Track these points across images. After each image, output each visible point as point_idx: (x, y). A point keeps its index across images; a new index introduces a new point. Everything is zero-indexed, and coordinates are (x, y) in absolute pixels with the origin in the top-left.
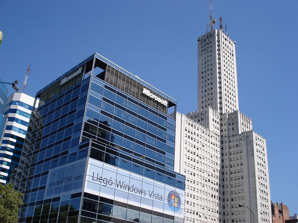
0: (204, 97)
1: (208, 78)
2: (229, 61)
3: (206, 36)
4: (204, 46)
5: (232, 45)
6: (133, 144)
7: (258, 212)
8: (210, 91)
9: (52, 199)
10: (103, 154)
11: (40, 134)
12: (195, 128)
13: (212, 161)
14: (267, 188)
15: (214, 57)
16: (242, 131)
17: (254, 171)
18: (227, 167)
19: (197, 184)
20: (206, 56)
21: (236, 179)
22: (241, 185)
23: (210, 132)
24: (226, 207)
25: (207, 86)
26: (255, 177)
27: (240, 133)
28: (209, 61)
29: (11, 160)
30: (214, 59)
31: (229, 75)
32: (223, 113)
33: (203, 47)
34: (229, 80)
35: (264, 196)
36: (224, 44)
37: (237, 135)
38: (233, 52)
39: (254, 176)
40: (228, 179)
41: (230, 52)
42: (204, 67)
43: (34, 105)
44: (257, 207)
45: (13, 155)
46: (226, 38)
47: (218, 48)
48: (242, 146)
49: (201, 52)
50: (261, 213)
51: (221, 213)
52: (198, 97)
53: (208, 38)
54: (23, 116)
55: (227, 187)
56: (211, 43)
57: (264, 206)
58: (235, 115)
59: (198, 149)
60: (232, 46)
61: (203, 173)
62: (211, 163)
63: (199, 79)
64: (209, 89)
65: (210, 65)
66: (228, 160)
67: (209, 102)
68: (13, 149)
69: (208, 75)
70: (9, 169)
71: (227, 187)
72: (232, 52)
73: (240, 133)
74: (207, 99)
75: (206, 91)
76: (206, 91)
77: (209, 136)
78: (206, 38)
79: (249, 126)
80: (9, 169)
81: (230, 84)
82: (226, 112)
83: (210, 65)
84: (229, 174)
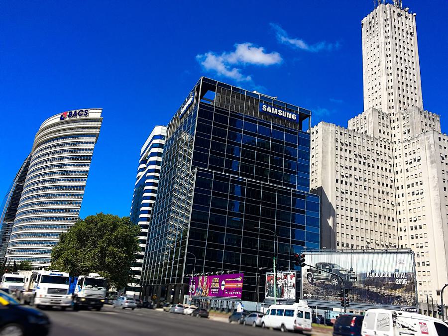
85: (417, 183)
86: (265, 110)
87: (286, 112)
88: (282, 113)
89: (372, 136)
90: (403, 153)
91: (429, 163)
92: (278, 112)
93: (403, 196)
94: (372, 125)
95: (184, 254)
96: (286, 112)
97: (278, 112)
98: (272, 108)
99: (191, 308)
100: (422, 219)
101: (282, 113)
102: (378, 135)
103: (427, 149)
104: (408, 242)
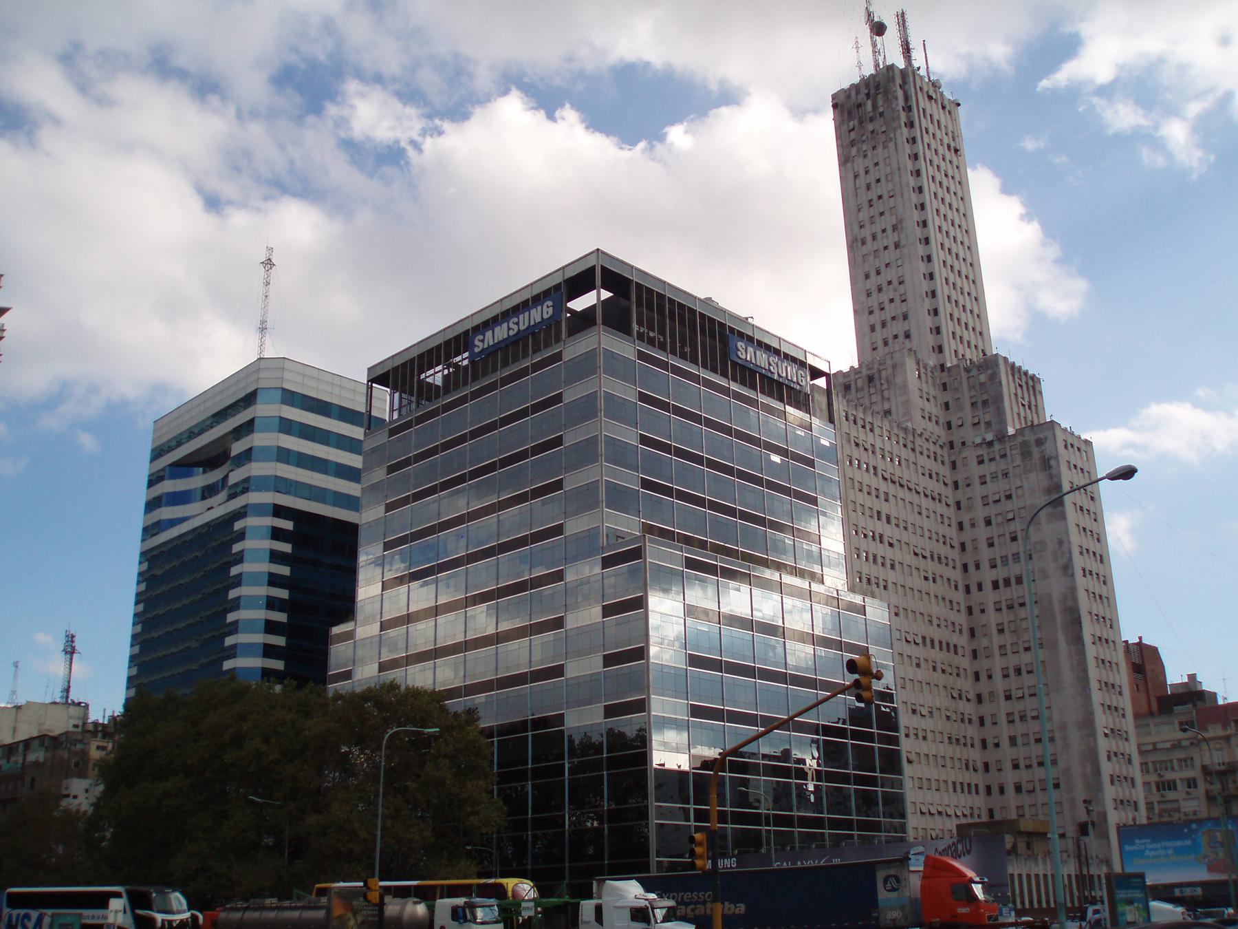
1: (893, 304)
2: (946, 175)
3: (864, 91)
4: (856, 128)
5: (949, 112)
6: (668, 418)
8: (895, 290)
9: (453, 340)
12: (863, 427)
13: (945, 623)
14: (1098, 520)
15: (899, 169)
16: (1018, 427)
18: (1000, 647)
19: (921, 788)
20: (869, 163)
23: (916, 436)
24: (958, 464)
25: (877, 220)
27: (1011, 431)
28: (883, 180)
30: (900, 177)
31: (948, 191)
32: (949, 365)
33: (853, 130)
34: (951, 229)
35: (1114, 701)
36: (925, 117)
38: (957, 139)
41: (946, 141)
42: (866, 205)
45: (287, 643)
46: (930, 94)
47: (914, 165)
50: (1106, 735)
51: (941, 423)
53: (868, 95)
54: (287, 479)
57: (1098, 597)
58: (989, 372)
59: (891, 545)
60: (961, 202)
62: (918, 454)
64: (890, 283)
65: (885, 196)
68: (289, 530)
69: (884, 231)
71: (960, 426)
72: (954, 140)
73: (1011, 431)
76: (874, 237)
77: (913, 450)
78: (862, 97)
79: (1033, 403)
81: (953, 225)
82: (955, 362)
83: (895, 282)
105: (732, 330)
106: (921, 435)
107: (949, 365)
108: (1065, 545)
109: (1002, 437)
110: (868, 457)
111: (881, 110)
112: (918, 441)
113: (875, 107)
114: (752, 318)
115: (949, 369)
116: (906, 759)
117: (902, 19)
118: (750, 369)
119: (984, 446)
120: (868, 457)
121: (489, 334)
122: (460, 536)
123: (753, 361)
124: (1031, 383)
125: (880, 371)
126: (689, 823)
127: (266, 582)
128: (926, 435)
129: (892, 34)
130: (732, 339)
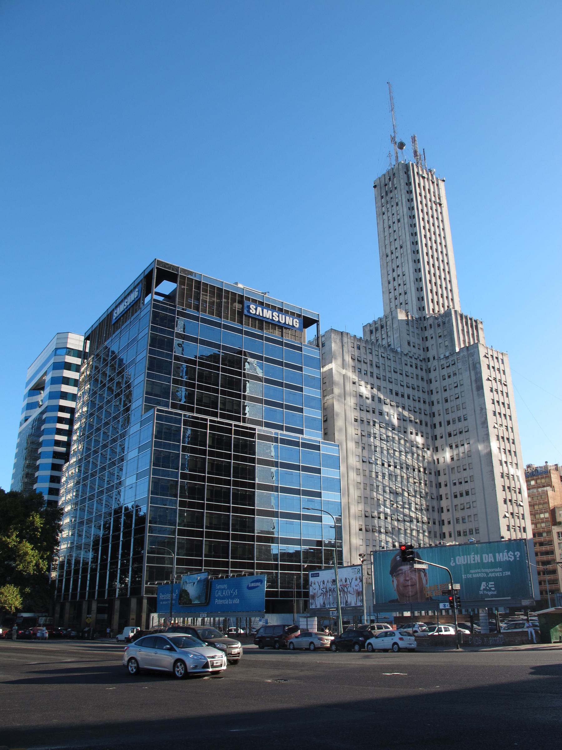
0: (392, 282)
7: (497, 489)
10: (238, 527)
11: (108, 414)
16: (462, 346)
17: (485, 416)
21: (470, 508)
22: (459, 385)
26: (487, 427)
27: (457, 350)
29: (69, 414)
37: (454, 354)
39: (485, 426)
40: (438, 379)
43: (85, 347)
44: (493, 480)
48: (461, 374)
49: (381, 216)
52: (383, 292)
55: (434, 370)
56: (396, 188)
61: (401, 375)
63: (381, 259)
66: (434, 347)
67: (398, 271)
70: (69, 417)
71: (434, 370)
74: (398, 295)
75: (394, 279)
78: (387, 180)
80: (69, 417)
84: (441, 392)
85: (449, 377)
86: (254, 312)
87: (284, 316)
88: (278, 316)
89: (399, 350)
90: (439, 374)
91: (474, 389)
92: (273, 316)
93: (441, 425)
94: (398, 335)
95: (99, 541)
96: (284, 316)
97: (273, 316)
98: (269, 311)
99: (345, 399)
100: (468, 469)
101: (278, 316)
102: (406, 349)
103: (471, 368)
104: (438, 374)
105: (248, 299)
106: (406, 355)
107: (428, 317)
108: (484, 411)
109: (453, 352)
110: (367, 367)
111: (396, 186)
112: (404, 358)
113: (393, 184)
114: (269, 292)
115: (428, 319)
116: (22, 426)
117: (414, 140)
118: (259, 320)
119: (444, 359)
120: (367, 367)
121: (118, 309)
122: (269, 455)
123: (261, 315)
124: (474, 324)
125: (386, 322)
126: (378, 624)
127: (52, 456)
128: (410, 355)
129: (408, 148)
130: (246, 303)
